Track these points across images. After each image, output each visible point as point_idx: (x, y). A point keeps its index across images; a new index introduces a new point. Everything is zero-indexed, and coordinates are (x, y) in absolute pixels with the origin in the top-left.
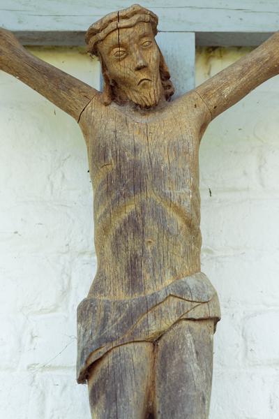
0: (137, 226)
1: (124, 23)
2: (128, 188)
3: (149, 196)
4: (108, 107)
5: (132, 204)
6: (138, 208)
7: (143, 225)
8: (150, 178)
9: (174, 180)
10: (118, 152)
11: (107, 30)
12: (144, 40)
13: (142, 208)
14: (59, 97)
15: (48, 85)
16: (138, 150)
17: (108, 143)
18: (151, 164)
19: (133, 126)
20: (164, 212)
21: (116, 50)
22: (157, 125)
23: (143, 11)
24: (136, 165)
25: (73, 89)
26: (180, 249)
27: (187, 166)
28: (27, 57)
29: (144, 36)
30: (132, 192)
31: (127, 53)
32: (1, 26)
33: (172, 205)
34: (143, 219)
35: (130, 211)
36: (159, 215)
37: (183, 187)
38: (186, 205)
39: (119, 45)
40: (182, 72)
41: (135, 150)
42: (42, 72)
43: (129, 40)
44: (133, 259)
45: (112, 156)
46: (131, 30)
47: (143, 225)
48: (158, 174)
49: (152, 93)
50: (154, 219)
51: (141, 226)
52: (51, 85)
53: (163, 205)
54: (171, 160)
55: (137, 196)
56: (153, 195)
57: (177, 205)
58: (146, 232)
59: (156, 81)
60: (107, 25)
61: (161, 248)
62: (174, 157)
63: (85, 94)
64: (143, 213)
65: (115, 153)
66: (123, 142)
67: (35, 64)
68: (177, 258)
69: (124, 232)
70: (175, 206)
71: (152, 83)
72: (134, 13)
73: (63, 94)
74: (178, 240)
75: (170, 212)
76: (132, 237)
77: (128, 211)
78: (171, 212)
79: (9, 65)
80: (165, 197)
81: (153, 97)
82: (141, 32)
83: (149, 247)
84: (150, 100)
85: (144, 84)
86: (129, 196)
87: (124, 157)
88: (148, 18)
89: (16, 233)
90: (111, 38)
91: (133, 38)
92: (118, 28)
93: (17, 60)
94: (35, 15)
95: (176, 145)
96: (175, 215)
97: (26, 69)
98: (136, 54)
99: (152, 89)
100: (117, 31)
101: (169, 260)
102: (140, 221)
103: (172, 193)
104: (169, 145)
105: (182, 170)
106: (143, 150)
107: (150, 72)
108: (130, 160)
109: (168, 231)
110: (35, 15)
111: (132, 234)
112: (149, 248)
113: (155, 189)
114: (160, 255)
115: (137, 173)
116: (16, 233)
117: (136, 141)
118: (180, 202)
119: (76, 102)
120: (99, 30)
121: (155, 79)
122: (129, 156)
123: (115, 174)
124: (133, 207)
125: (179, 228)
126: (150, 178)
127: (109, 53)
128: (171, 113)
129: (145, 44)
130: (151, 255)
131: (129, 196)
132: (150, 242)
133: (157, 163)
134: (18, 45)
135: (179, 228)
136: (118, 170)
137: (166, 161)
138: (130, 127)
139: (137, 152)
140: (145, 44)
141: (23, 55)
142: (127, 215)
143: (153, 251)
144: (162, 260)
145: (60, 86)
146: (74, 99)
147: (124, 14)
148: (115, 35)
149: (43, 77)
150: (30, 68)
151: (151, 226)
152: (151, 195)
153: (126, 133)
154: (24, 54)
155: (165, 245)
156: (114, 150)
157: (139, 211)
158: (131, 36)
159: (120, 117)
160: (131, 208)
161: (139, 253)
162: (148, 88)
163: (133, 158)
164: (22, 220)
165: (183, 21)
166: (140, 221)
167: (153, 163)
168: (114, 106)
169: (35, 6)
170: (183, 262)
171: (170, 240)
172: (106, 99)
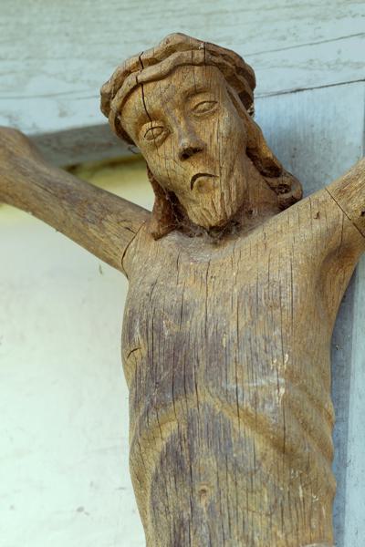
0: (179, 462)
1: (150, 72)
2: (163, 391)
3: (201, 399)
4: (159, 242)
5: (170, 420)
6: (183, 427)
7: (191, 459)
8: (203, 364)
9: (244, 362)
10: (150, 322)
11: (121, 93)
12: (199, 99)
13: (190, 425)
14: (88, 237)
15: (69, 219)
16: (187, 314)
17: (137, 307)
18: (206, 337)
19: (187, 267)
20: (227, 429)
21: (148, 125)
22: (227, 261)
23: (184, 44)
24: (180, 343)
25: (108, 217)
26: (262, 497)
27: (277, 332)
28: (37, 172)
29: (196, 92)
30: (169, 396)
31: (166, 132)
32: (4, 122)
33: (241, 412)
34: (190, 447)
35: (169, 434)
36: (220, 436)
37: (264, 374)
38: (269, 408)
39: (149, 117)
40: (339, 160)
41: (183, 314)
42: (61, 195)
43: (163, 104)
44: (177, 530)
45: (141, 332)
46: (164, 83)
47: (191, 459)
48: (217, 355)
49: (217, 201)
50: (210, 445)
51: (186, 460)
52: (73, 217)
53: (226, 414)
54: (242, 324)
55: (178, 404)
56: (208, 399)
57: (251, 410)
58: (195, 473)
59: (229, 176)
60: (122, 82)
61: (224, 501)
62: (248, 316)
63: (126, 224)
64: (191, 436)
65: (144, 325)
66: (161, 301)
67: (49, 183)
68: (257, 517)
69: (161, 478)
70: (247, 414)
71: (218, 181)
72: (169, 51)
73: (93, 230)
74: (257, 482)
75: (241, 428)
76: (173, 485)
77: (166, 434)
78: (242, 426)
79: (10, 193)
80: (229, 397)
81: (218, 207)
82: (187, 85)
83: (203, 502)
84: (213, 215)
85: (200, 185)
86: (165, 406)
87: (160, 331)
88: (199, 55)
89: (80, 510)
90: (132, 106)
91: (169, 99)
92: (140, 84)
93: (21, 180)
94: (88, 98)
95: (253, 294)
96: (249, 432)
97: (35, 194)
98: (179, 128)
99: (218, 193)
100: (140, 90)
101: (241, 522)
102: (185, 452)
103: (240, 389)
104: (240, 293)
105: (262, 341)
106: (196, 313)
107: (212, 160)
108: (171, 335)
109: (235, 465)
110: (88, 98)
111: (172, 479)
112: (202, 504)
113: (210, 384)
114: (222, 514)
115: (181, 357)
116: (80, 510)
117: (185, 298)
118: (255, 404)
119: (112, 242)
120: (110, 93)
121: (224, 172)
122: (168, 326)
123: (145, 365)
124: (174, 425)
125: (258, 458)
126: (203, 364)
127: (137, 133)
128: (261, 234)
129: (201, 107)
130: (206, 518)
131: (165, 406)
132: (204, 491)
133: (217, 334)
134: (25, 154)
135: (258, 458)
136: (150, 359)
137: (233, 327)
138: (181, 271)
139: (184, 317)
140: (201, 107)
141: (61, 176)
142: (164, 443)
143: (210, 508)
144: (226, 526)
145: (88, 217)
146: (108, 237)
147: (150, 55)
148: (136, 98)
149: (61, 204)
150: (41, 191)
151: (207, 460)
152: (206, 397)
153: (173, 284)
154: (33, 168)
155: (232, 494)
156: (144, 319)
157: (185, 432)
158: (165, 95)
159: (171, 255)
160: (170, 429)
161: (186, 514)
162: (209, 191)
163: (176, 329)
164: (92, 484)
165: (345, 64)
166: (185, 452)
167: (210, 335)
168: (174, 237)
169: (89, 81)
170: (271, 525)
171: (240, 482)
172: (154, 227)
